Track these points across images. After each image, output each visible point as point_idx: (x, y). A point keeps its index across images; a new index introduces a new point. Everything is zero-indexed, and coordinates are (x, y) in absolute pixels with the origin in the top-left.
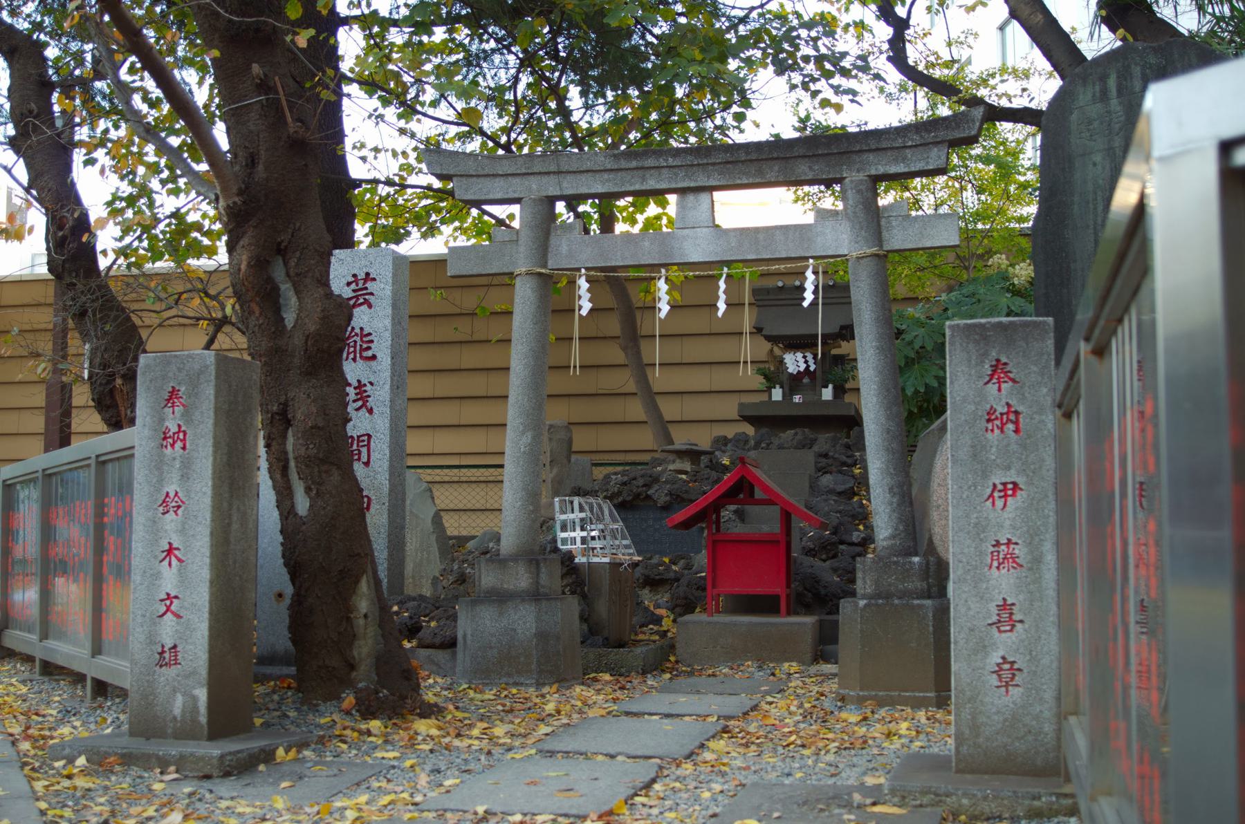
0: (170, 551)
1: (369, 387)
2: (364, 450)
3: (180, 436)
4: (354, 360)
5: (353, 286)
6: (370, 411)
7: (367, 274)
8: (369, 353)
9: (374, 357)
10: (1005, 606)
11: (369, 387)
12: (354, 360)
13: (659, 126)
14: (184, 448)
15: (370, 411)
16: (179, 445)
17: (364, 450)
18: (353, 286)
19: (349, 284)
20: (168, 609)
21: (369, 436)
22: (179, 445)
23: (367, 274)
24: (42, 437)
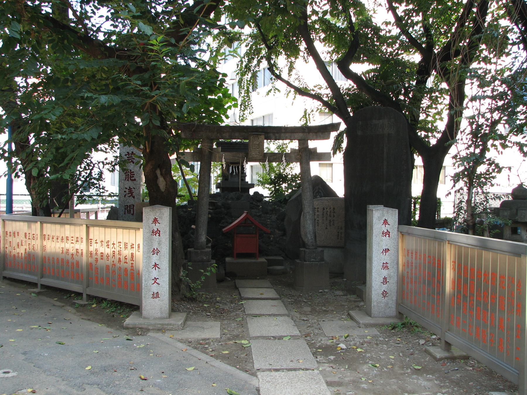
0: (156, 265)
1: (133, 189)
2: (132, 210)
3: (158, 232)
4: (128, 180)
5: (127, 156)
6: (134, 197)
7: (132, 152)
8: (133, 178)
9: (135, 180)
10: (385, 278)
11: (133, 189)
12: (128, 180)
13: (44, 18)
14: (159, 236)
15: (134, 197)
16: (158, 234)
17: (132, 210)
18: (127, 156)
19: (126, 155)
20: (155, 282)
21: (134, 206)
22: (158, 234)
23: (132, 152)
24: (14, 193)
